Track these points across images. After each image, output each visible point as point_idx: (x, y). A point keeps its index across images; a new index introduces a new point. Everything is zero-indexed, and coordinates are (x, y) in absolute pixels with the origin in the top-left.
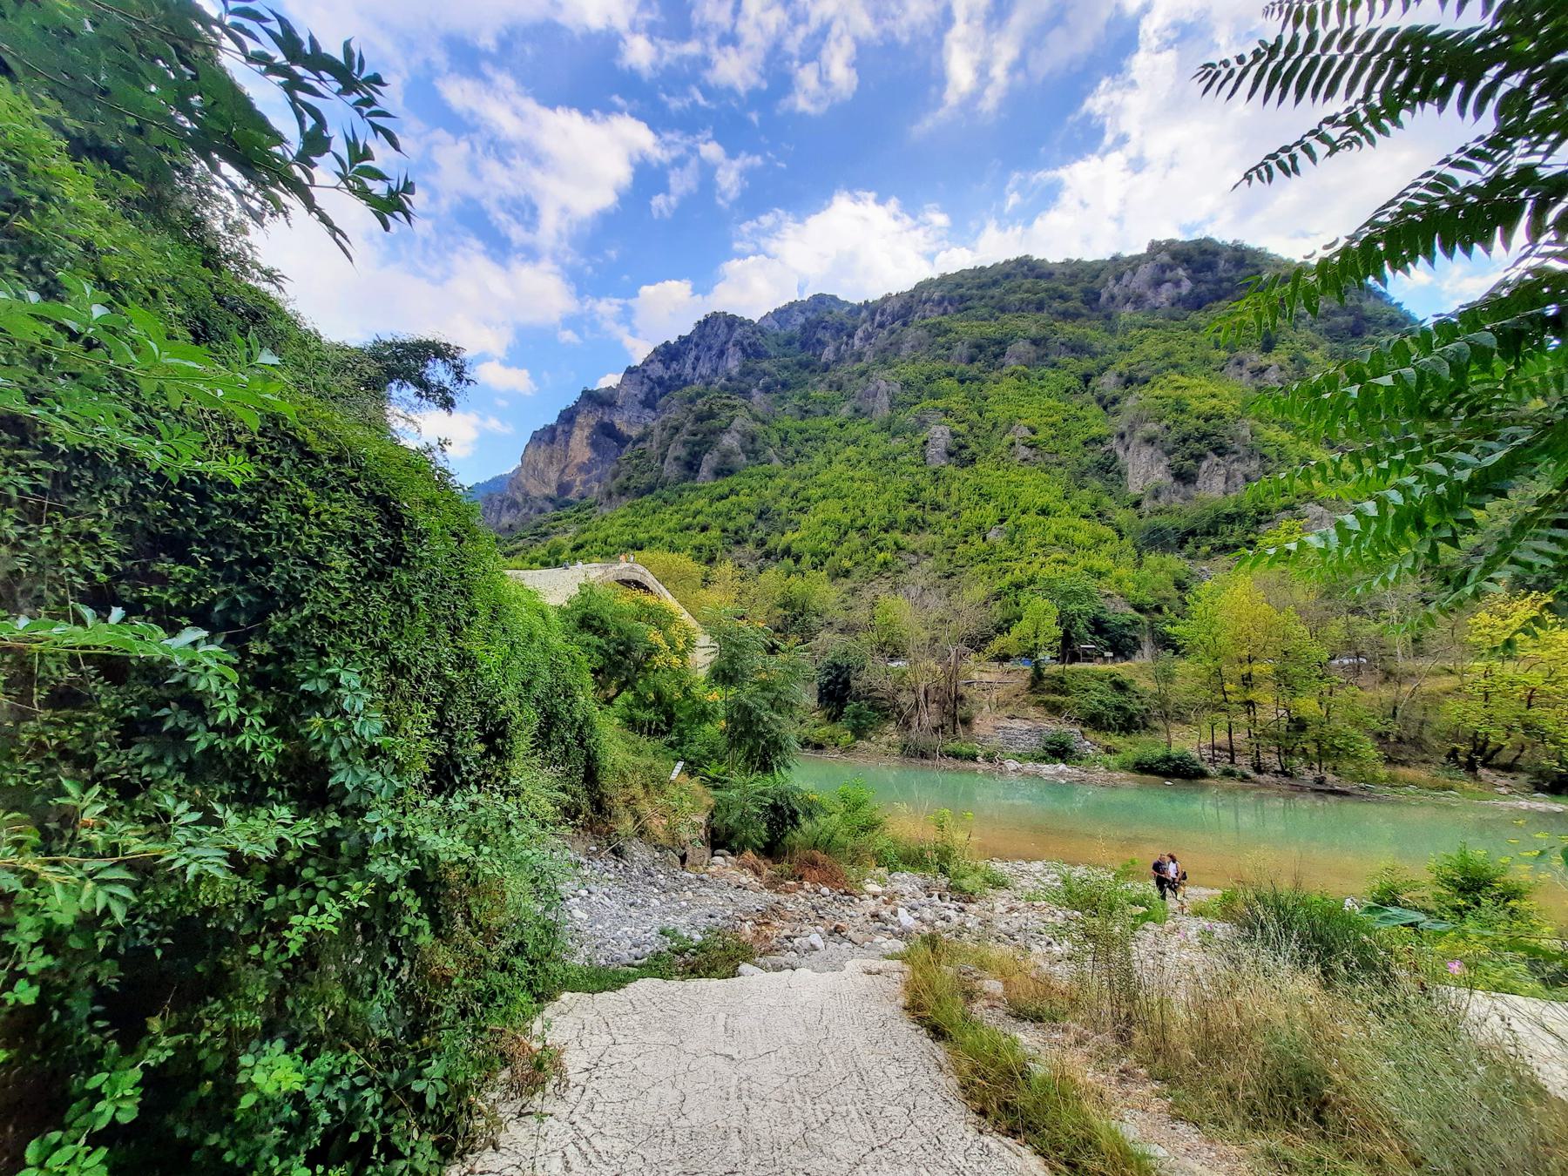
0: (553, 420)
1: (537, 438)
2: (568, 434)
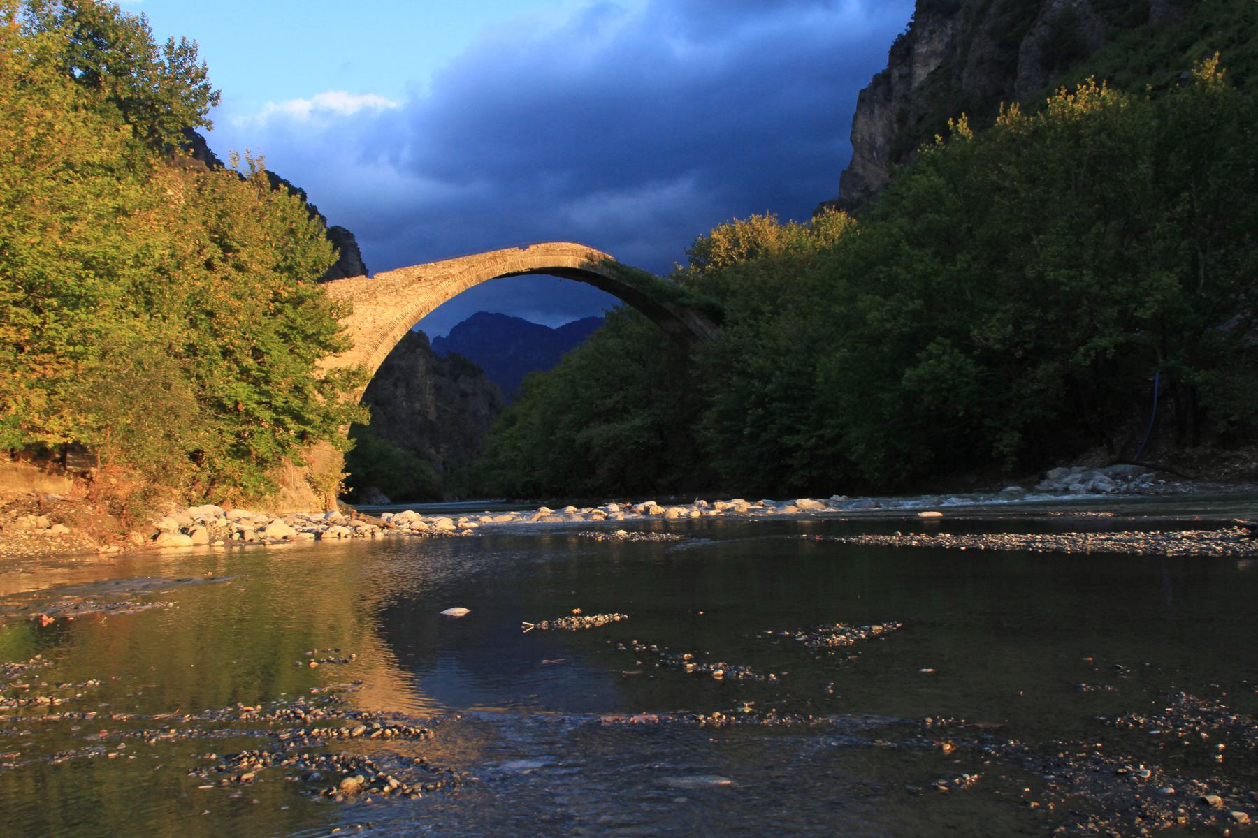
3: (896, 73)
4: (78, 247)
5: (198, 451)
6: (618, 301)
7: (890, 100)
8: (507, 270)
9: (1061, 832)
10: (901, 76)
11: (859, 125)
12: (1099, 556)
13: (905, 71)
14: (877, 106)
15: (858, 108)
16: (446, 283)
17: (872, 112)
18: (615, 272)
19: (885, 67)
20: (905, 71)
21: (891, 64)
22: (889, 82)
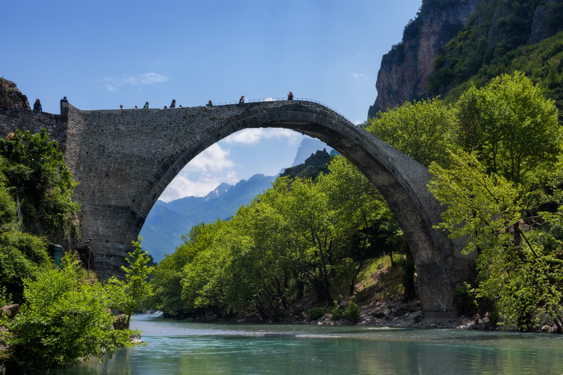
0: (398, 39)
1: (387, 61)
2: (415, 48)
7: (403, 62)
10: (410, 46)
13: (413, 43)
14: (394, 65)
15: (382, 66)
17: (391, 69)
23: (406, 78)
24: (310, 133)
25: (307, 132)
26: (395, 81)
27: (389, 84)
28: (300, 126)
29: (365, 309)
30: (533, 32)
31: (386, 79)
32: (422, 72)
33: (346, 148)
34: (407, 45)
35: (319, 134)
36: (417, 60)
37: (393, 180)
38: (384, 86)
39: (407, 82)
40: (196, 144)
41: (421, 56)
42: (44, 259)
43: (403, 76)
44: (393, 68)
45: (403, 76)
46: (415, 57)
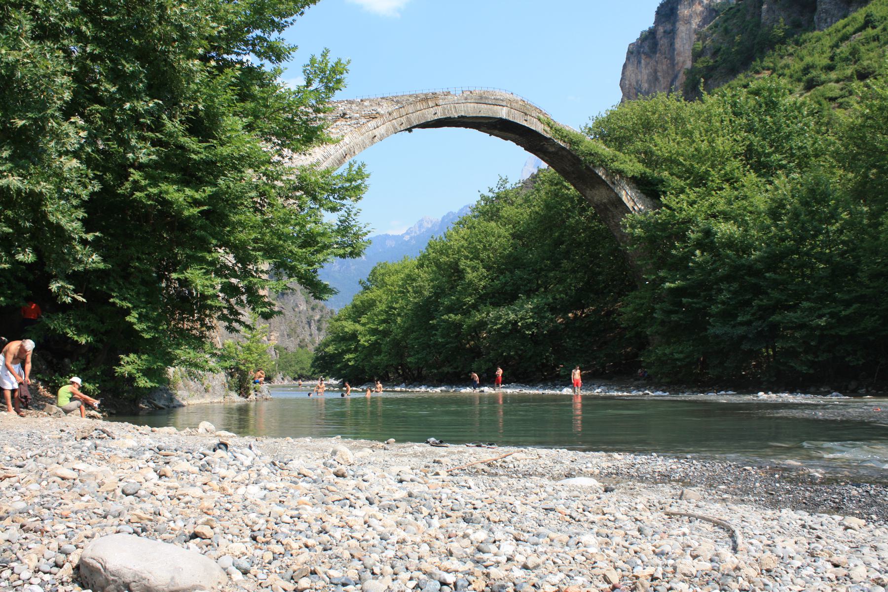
0: (648, 21)
2: (671, 34)
3: (661, 30)
4: (151, 157)
5: (55, 562)
6: (544, 165)
7: (655, 53)
8: (440, 116)
9: (21, 119)
10: (665, 32)
11: (628, 73)
12: (532, 383)
13: (668, 27)
14: (643, 57)
15: (628, 59)
16: (373, 123)
17: (639, 62)
18: (548, 129)
19: (652, 25)
20: (668, 27)
21: (657, 22)
22: (654, 38)
23: (659, 74)
24: (502, 133)
25: (496, 132)
26: (646, 77)
27: (637, 83)
28: (486, 124)
29: (813, 481)
30: (819, 8)
31: (633, 75)
32: (680, 64)
33: (550, 153)
34: (661, 30)
35: (510, 135)
36: (674, 50)
37: (613, 195)
38: (630, 85)
39: (661, 79)
40: (344, 148)
41: (678, 44)
42: (203, 342)
43: (656, 71)
44: (643, 61)
45: (656, 71)
46: (672, 44)
